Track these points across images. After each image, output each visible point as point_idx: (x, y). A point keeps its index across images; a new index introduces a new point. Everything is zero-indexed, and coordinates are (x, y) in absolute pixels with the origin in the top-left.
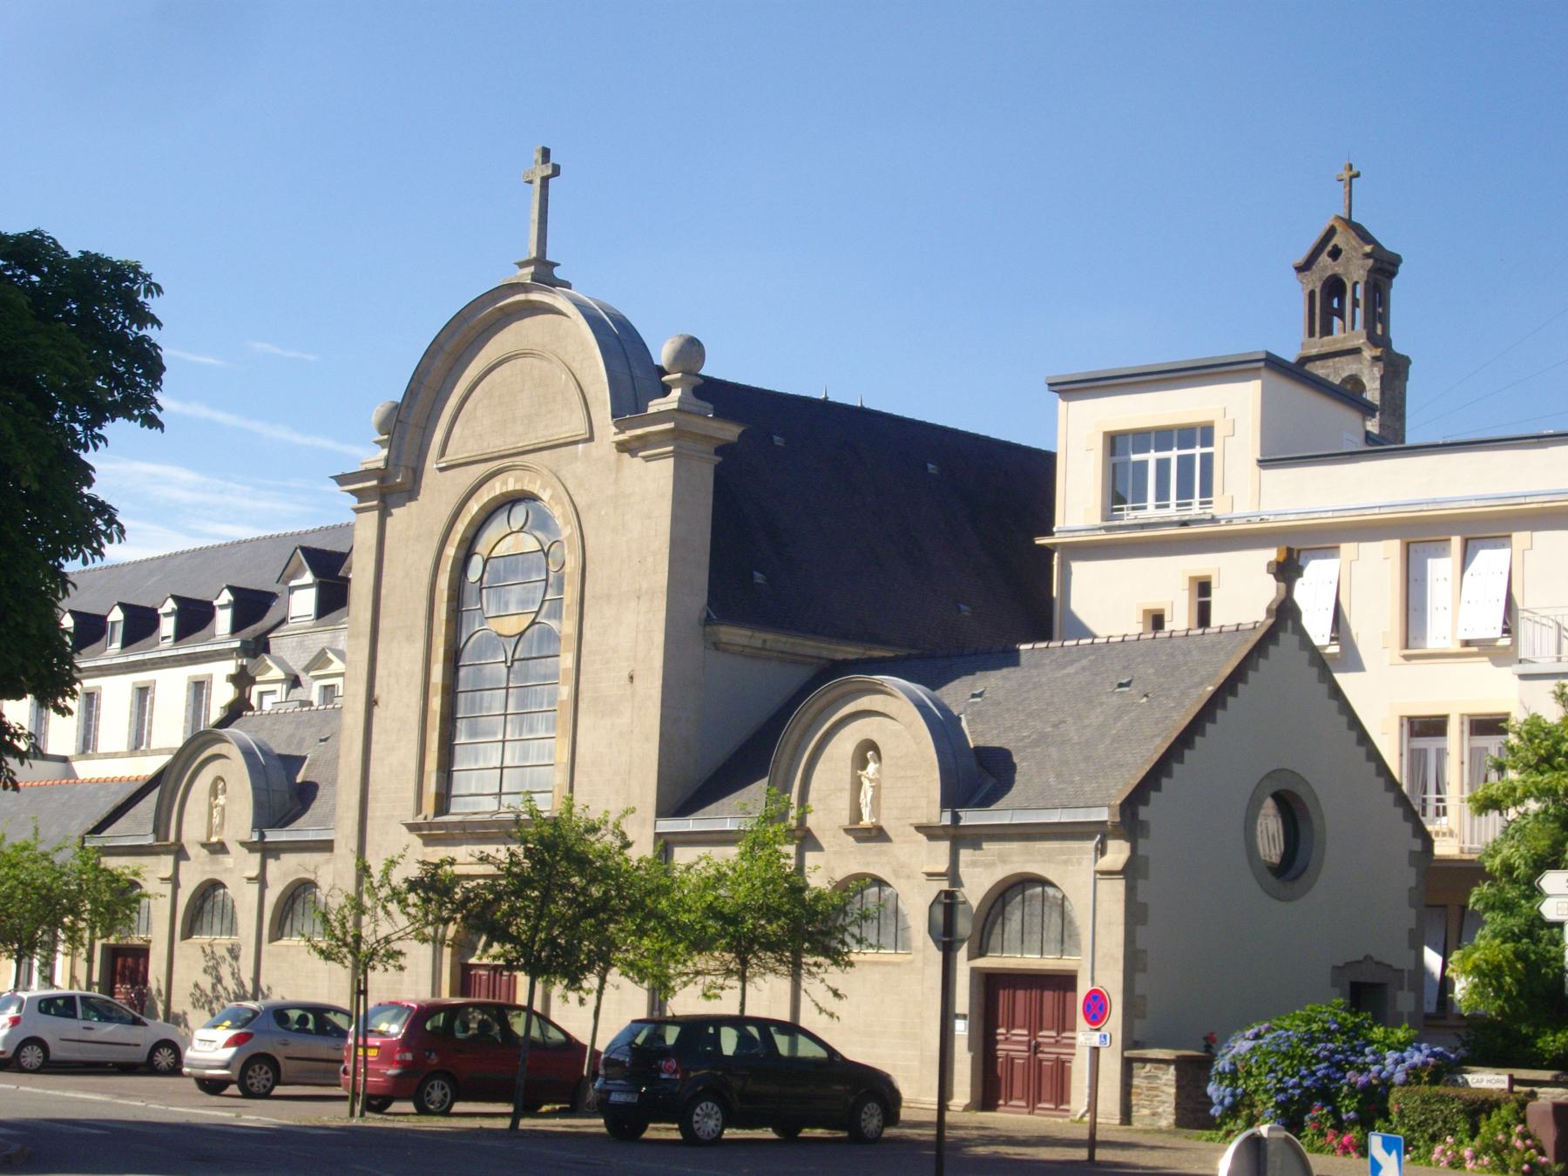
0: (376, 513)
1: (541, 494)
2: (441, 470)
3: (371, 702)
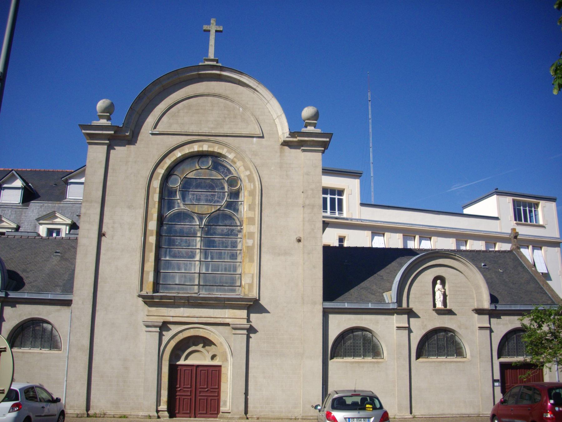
0: (106, 147)
1: (227, 154)
2: (153, 134)
3: (101, 234)
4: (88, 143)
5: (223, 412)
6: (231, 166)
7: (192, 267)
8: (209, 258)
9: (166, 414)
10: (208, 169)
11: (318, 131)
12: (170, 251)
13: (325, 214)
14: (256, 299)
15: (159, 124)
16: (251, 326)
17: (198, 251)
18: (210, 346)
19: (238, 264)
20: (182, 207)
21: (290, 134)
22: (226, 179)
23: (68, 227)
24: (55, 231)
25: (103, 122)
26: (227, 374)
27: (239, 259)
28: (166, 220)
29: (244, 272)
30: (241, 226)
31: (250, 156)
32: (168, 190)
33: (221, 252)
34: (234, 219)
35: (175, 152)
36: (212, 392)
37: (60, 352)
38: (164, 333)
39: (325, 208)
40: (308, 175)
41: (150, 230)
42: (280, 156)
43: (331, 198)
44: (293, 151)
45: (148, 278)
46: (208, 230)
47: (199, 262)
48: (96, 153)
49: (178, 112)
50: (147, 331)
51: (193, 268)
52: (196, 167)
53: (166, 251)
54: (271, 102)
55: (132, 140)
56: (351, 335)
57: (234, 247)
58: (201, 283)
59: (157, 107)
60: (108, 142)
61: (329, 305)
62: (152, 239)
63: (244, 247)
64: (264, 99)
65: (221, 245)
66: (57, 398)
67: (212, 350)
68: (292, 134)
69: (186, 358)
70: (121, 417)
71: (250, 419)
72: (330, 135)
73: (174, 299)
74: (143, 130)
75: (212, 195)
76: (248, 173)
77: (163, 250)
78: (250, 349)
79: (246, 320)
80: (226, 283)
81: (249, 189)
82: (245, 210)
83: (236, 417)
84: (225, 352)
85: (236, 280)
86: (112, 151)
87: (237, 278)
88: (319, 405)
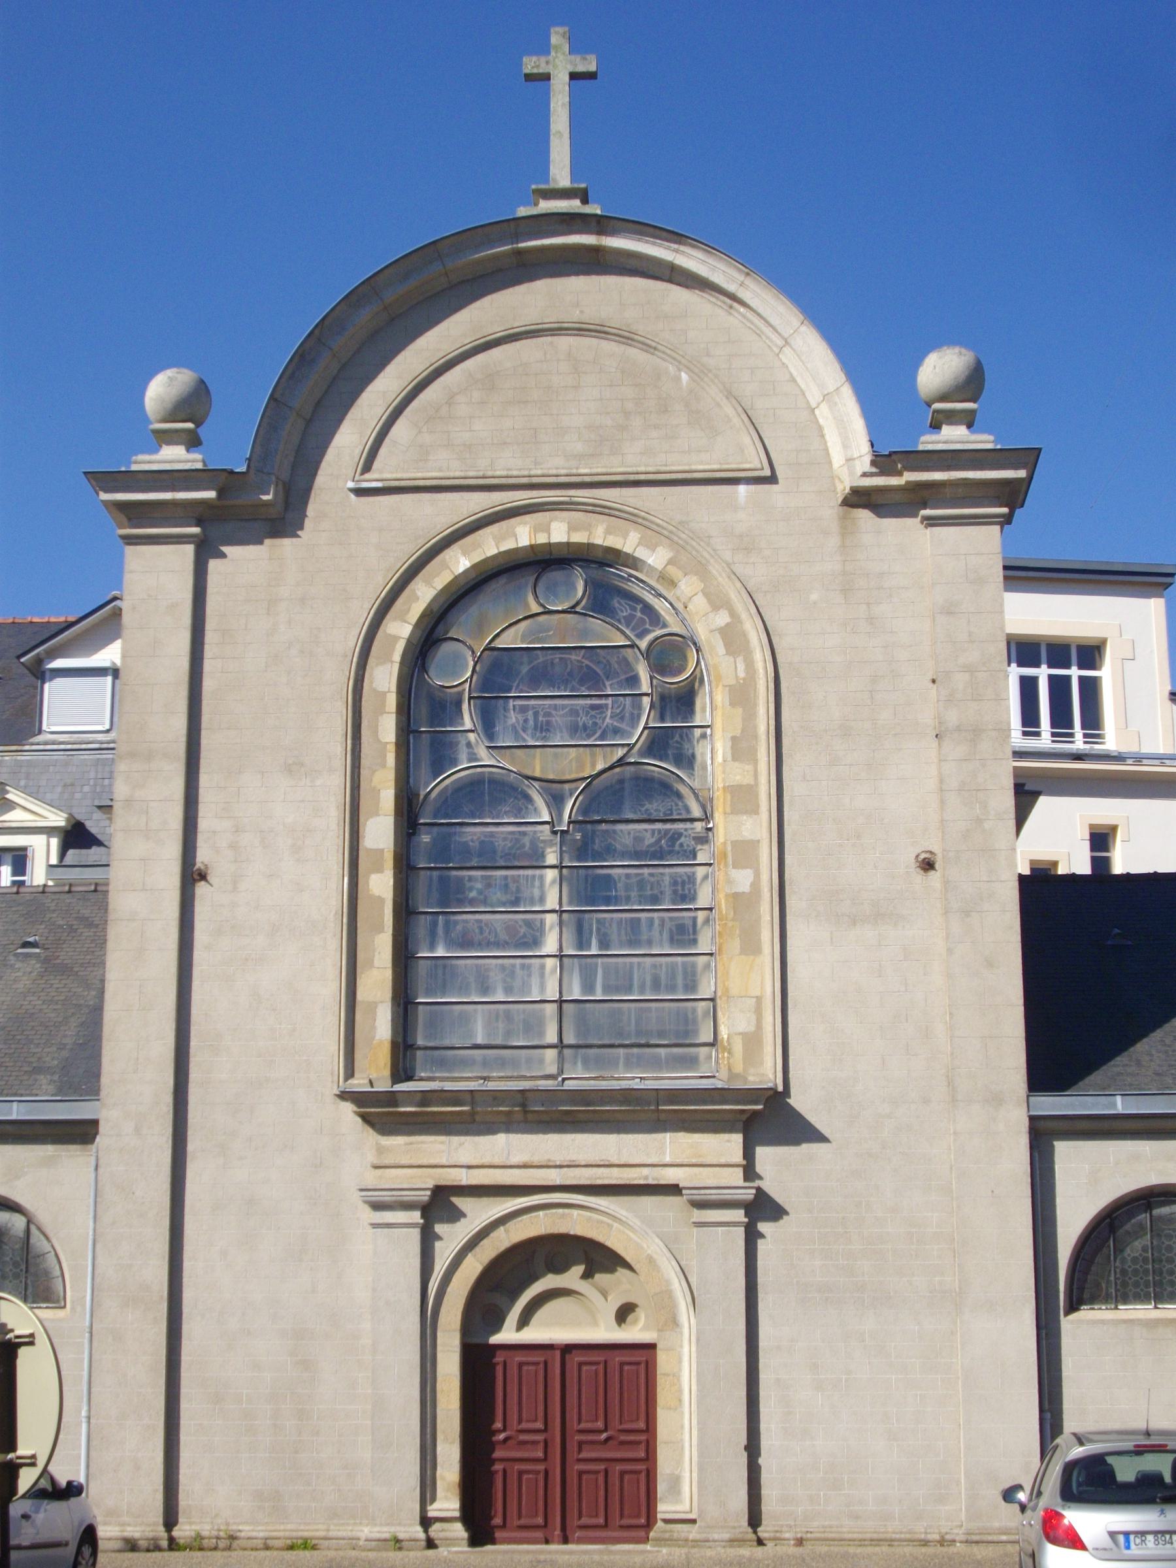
0: (189, 549)
1: (641, 553)
2: (360, 492)
3: (192, 876)
4: (123, 537)
5: (666, 1521)
6: (659, 595)
7: (532, 979)
8: (594, 942)
9: (458, 1530)
10: (571, 611)
11: (984, 441)
12: (447, 924)
13: (1031, 744)
14: (774, 1090)
15: (383, 451)
16: (759, 1189)
17: (551, 919)
18: (611, 1270)
19: (702, 960)
20: (485, 758)
21: (873, 463)
22: (643, 644)
23: (55, 842)
24: (8, 857)
25: (174, 456)
26: (677, 1377)
27: (704, 946)
28: (429, 808)
29: (727, 990)
30: (706, 818)
31: (727, 556)
32: (431, 698)
33: (639, 919)
34: (679, 795)
35: (449, 554)
36: (622, 1443)
37: (60, 1314)
38: (439, 1228)
39: (1030, 718)
40: (950, 613)
41: (368, 850)
42: (843, 546)
43: (1051, 678)
44: (892, 525)
45: (374, 1028)
46: (586, 842)
47: (556, 961)
48: (156, 575)
49: (450, 402)
50: (375, 1226)
51: (535, 982)
52: (527, 606)
53: (434, 924)
54: (798, 342)
55: (284, 520)
56: (1144, 1217)
57: (684, 898)
58: (569, 1039)
59: (370, 388)
60: (196, 530)
61: (1053, 1105)
62: (381, 885)
63: (721, 896)
64: (768, 331)
65: (634, 894)
66: (69, 1483)
67: (618, 1286)
68: (883, 462)
69: (523, 1322)
70: (291, 1548)
71: (770, 1544)
72: (1029, 457)
73: (473, 1103)
74: (322, 479)
75: (593, 707)
76: (722, 619)
77: (422, 923)
78: (761, 1279)
79: (739, 1172)
80: (661, 1034)
81: (733, 682)
82: (719, 758)
83: (716, 1536)
84: (668, 1292)
85: (695, 1021)
86: (213, 565)
87: (700, 1012)
88: (1019, 1487)
